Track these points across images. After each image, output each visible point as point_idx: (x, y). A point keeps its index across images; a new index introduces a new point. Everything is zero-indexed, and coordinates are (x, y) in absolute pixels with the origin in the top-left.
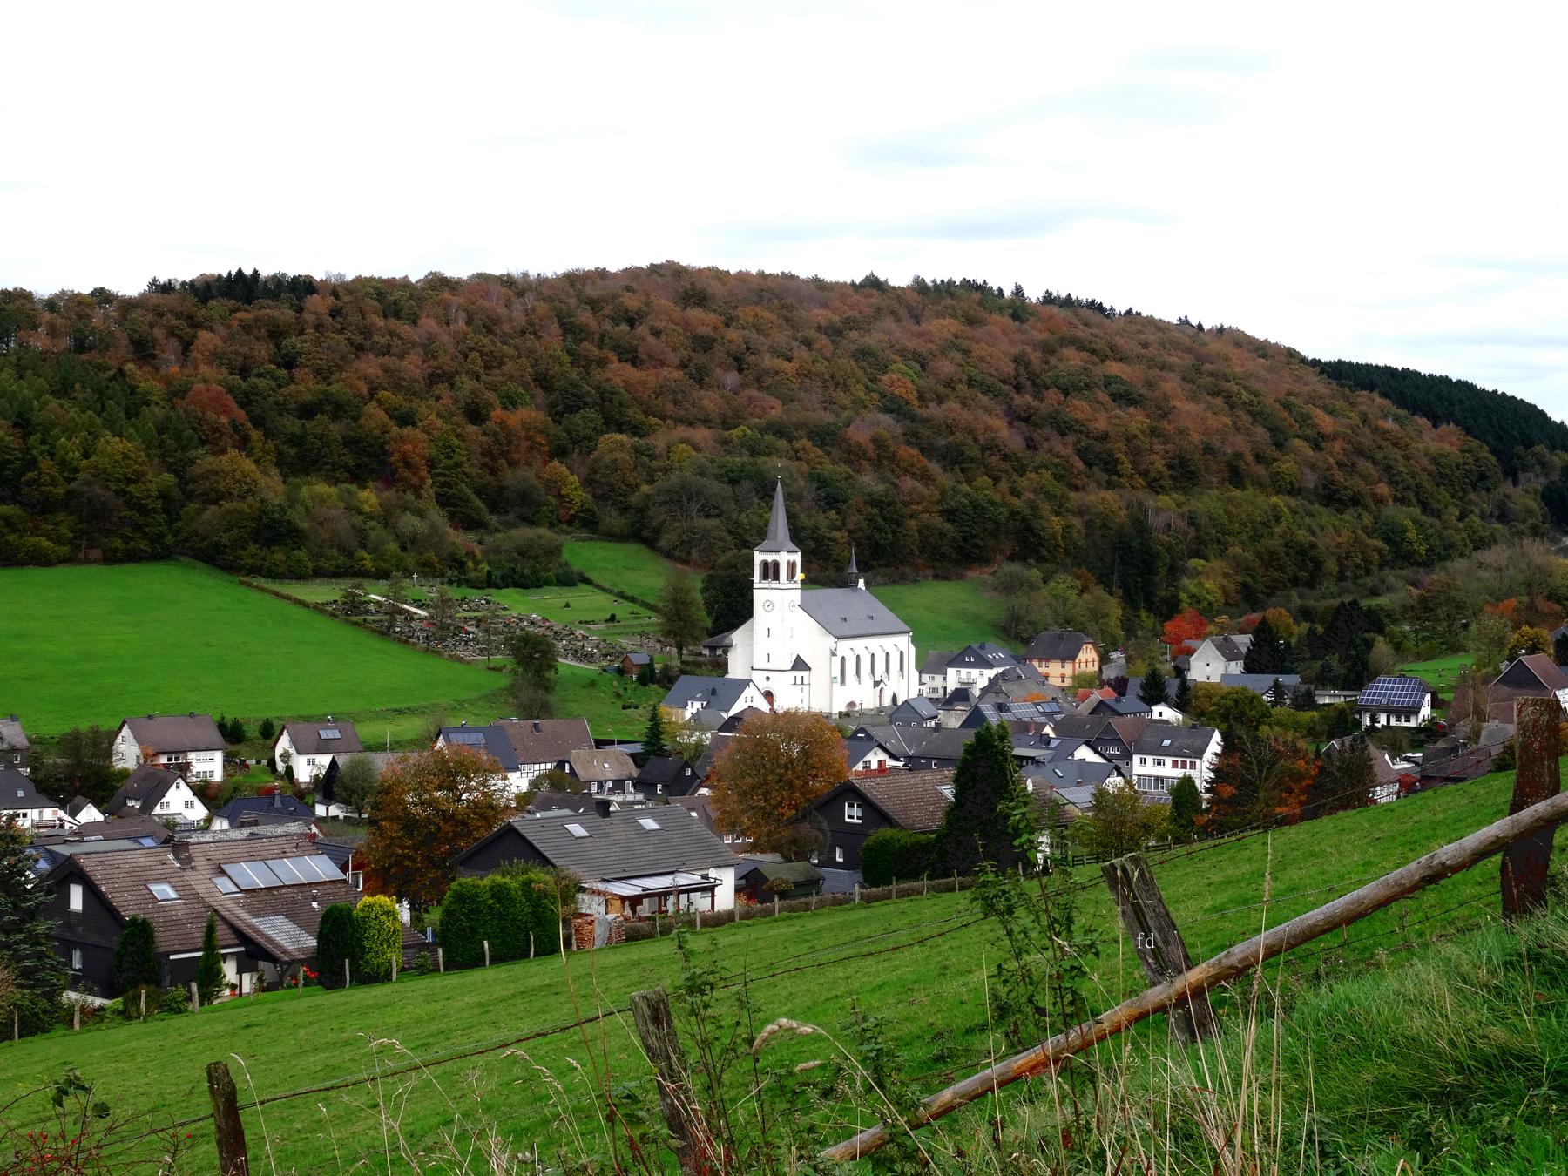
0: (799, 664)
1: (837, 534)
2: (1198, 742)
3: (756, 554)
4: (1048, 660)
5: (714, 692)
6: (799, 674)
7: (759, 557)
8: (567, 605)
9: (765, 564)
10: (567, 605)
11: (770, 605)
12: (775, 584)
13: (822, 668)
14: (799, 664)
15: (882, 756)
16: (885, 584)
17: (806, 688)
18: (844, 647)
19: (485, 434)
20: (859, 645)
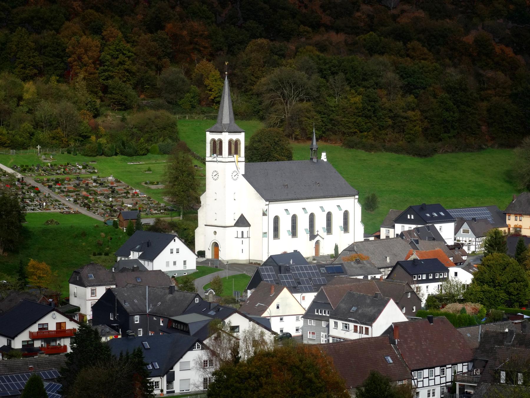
0: (242, 222)
1: (410, 113)
2: (370, 310)
3: (208, 133)
4: (521, 215)
5: (148, 244)
6: (240, 229)
7: (210, 136)
8: (149, 170)
9: (214, 142)
10: (149, 170)
11: (216, 174)
12: (219, 159)
13: (260, 225)
14: (242, 222)
15: (61, 318)
16: (453, 151)
17: (246, 241)
18: (277, 208)
19: (154, 40)
20: (295, 207)
